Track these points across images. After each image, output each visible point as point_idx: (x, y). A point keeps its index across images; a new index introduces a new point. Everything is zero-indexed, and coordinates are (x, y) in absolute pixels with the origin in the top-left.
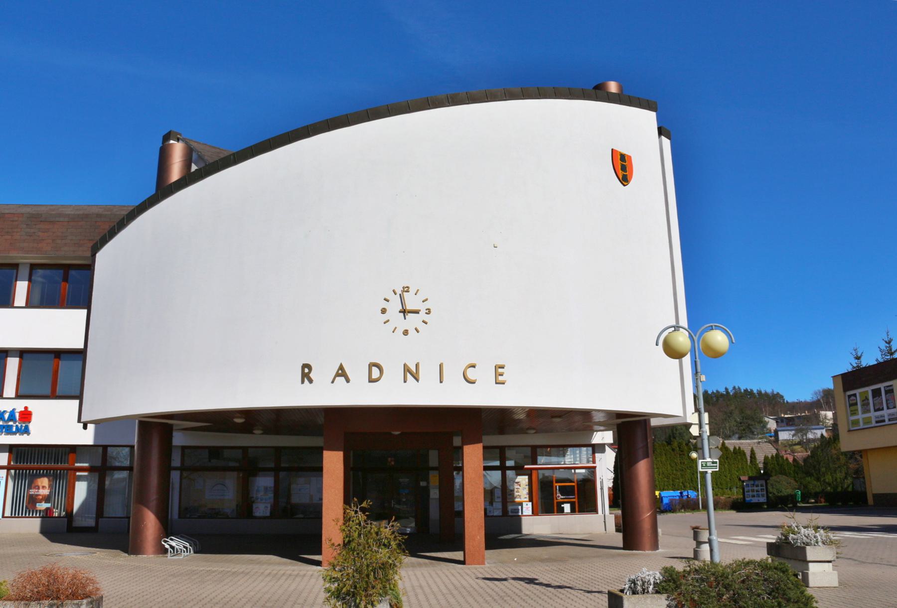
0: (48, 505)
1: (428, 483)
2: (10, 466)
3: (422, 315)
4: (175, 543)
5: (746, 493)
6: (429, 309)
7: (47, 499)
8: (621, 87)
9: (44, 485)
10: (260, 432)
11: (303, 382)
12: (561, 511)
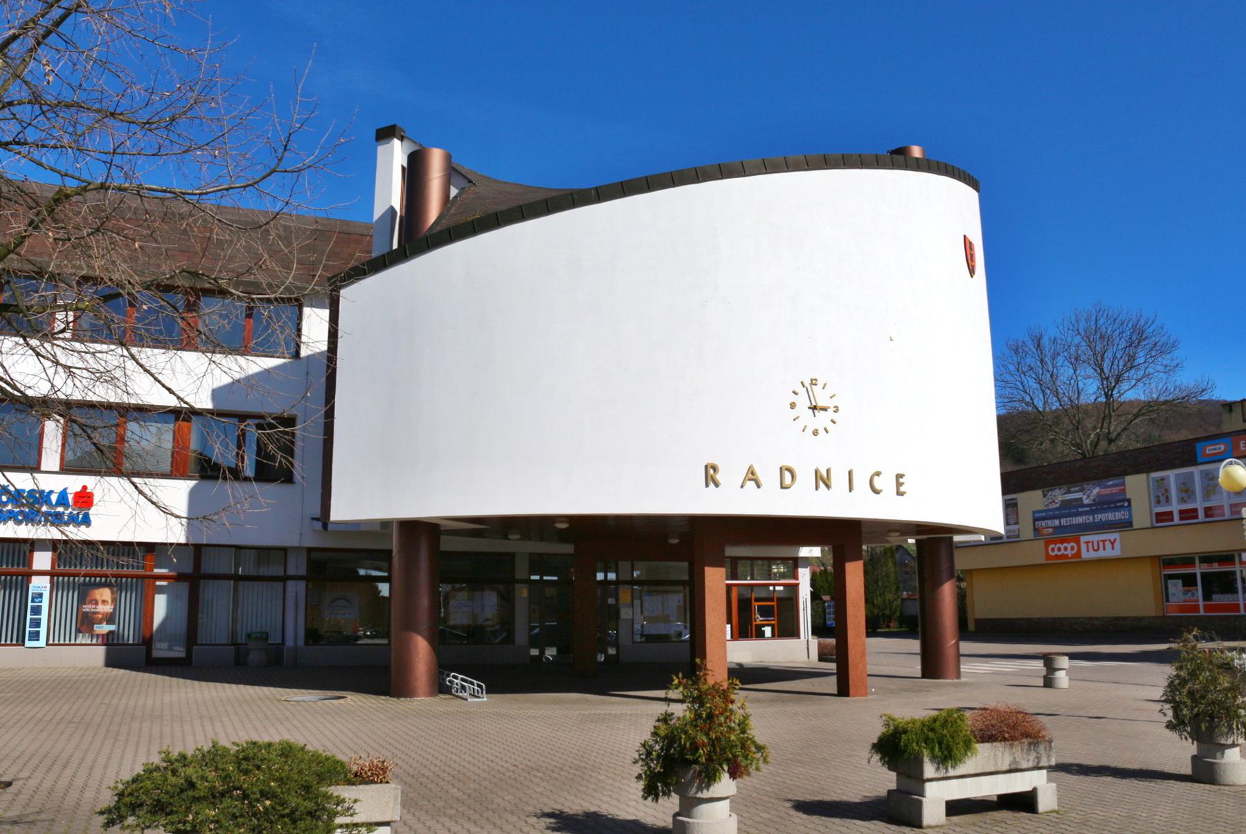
0: (112, 627)
1: (617, 600)
2: (54, 571)
3: (830, 414)
4: (456, 680)
5: (827, 616)
6: (837, 407)
7: (110, 619)
8: (924, 152)
9: (104, 598)
10: (518, 537)
11: (707, 485)
12: (760, 635)
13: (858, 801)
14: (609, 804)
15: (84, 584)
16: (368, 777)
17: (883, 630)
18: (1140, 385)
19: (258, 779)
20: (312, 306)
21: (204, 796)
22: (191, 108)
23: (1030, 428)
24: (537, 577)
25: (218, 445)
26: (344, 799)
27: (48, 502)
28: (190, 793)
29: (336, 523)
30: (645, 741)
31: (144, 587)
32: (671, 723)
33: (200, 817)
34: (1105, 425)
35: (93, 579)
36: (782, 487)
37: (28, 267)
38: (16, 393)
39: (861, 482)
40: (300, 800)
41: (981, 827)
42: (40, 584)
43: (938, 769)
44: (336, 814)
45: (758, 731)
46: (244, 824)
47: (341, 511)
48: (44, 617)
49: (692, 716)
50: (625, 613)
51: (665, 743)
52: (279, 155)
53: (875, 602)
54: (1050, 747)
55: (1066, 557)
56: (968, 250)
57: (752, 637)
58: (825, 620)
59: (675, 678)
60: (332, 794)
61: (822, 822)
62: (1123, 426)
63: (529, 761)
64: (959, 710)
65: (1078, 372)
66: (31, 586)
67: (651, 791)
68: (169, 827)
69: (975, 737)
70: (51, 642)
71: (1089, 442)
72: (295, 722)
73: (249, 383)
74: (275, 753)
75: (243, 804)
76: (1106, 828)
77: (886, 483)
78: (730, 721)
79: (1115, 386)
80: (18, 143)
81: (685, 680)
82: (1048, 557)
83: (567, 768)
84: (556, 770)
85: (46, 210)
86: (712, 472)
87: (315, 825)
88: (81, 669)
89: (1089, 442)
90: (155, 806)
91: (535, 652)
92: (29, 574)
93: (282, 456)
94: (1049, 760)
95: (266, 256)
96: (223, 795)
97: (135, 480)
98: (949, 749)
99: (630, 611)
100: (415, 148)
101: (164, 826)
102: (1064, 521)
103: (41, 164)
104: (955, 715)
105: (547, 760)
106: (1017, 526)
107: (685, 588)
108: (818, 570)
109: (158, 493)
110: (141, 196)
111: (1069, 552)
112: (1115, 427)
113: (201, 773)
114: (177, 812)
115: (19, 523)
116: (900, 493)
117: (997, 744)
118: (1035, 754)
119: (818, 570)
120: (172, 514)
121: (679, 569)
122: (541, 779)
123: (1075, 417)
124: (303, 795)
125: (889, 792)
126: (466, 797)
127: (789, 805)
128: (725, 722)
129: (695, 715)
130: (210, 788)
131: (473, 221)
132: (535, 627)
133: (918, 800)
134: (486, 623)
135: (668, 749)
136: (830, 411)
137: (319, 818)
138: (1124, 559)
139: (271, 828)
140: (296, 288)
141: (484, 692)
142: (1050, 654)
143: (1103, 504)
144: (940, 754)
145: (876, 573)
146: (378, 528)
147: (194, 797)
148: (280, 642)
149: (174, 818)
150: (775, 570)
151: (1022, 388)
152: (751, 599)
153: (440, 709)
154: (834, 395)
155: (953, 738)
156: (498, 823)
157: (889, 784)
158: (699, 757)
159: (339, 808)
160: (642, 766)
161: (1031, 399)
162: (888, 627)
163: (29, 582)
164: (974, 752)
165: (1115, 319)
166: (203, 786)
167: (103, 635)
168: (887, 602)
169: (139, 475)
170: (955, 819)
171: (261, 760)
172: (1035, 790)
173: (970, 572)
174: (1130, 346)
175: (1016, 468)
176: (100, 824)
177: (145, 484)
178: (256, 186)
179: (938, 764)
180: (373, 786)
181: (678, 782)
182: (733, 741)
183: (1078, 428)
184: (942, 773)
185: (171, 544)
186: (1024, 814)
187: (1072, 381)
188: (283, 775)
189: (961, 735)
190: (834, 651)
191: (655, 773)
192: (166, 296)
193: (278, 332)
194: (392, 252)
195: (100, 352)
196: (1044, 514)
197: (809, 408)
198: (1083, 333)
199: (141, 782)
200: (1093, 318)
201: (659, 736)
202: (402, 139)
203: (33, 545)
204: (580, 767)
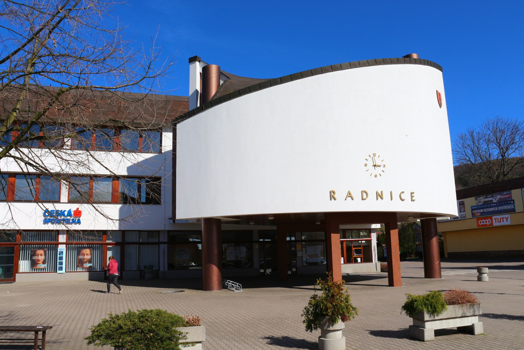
0: (91, 265)
1: (296, 248)
2: (67, 242)
3: (382, 168)
4: (230, 283)
6: (384, 165)
7: (90, 261)
8: (418, 56)
9: (87, 253)
10: (253, 223)
11: (331, 200)
13: (397, 330)
14: (292, 333)
15: (79, 247)
16: (192, 323)
17: (408, 258)
18: (517, 151)
19: (147, 325)
20: (166, 132)
21: (126, 332)
22: (112, 54)
23: (469, 171)
24: (262, 240)
25: (126, 190)
26: (182, 332)
27: (64, 215)
28: (120, 331)
29: (178, 220)
30: (306, 307)
31: (103, 248)
32: (317, 299)
33: (125, 340)
34: (502, 168)
35: (80, 245)
36: (362, 199)
37: (50, 121)
38: (46, 172)
39: (396, 196)
40: (164, 333)
41: (450, 341)
42: (62, 248)
43: (430, 317)
44: (179, 339)
45: (353, 302)
46: (142, 343)
47: (180, 215)
48: (64, 261)
49: (325, 296)
50: (299, 254)
51: (314, 308)
52: (147, 71)
53: (405, 246)
54: (479, 307)
55: (486, 225)
56: (439, 97)
57: (352, 262)
58: (383, 254)
59: (318, 280)
60: (177, 331)
61: (381, 339)
62: (510, 169)
63: (260, 316)
64: (439, 291)
65: (489, 146)
66: (58, 248)
67: (309, 327)
68: (112, 344)
69: (446, 303)
70: (67, 271)
71: (495, 176)
72: (164, 302)
73: (139, 164)
74: (154, 314)
75: (142, 335)
76: (505, 341)
77: (406, 196)
78: (341, 298)
79: (506, 152)
80: (43, 72)
81: (322, 281)
82: (478, 225)
83: (275, 318)
84: (270, 319)
85: (55, 98)
86: (333, 194)
87: (171, 343)
88: (79, 281)
89: (495, 176)
90: (107, 336)
91: (262, 271)
92: (58, 244)
93: (152, 193)
94: (479, 312)
95: (143, 112)
96: (133, 331)
97: (94, 205)
98: (435, 308)
99: (301, 253)
100: (205, 65)
101: (110, 344)
102: (485, 210)
103: (54, 80)
104: (437, 293)
105: (267, 315)
106: (464, 213)
107: (324, 243)
108: (380, 234)
109: (104, 210)
110: (92, 90)
111: (488, 223)
112: (506, 169)
113: (124, 323)
114: (115, 338)
115: (53, 223)
116: (412, 200)
117: (456, 306)
118: (473, 310)
119: (380, 234)
120: (109, 219)
121: (321, 235)
122: (264, 323)
123: (488, 166)
124: (165, 331)
125: (410, 326)
126: (233, 331)
127: (368, 332)
128: (339, 298)
129: (326, 296)
130: (128, 329)
131: (230, 94)
132: (262, 261)
133: (422, 329)
134: (242, 259)
135: (316, 310)
136: (382, 167)
137: (172, 340)
138: (512, 225)
139: (153, 344)
140: (156, 124)
141: (241, 287)
142: (480, 267)
143: (501, 203)
144: (431, 310)
145: (405, 234)
146: (195, 222)
147: (122, 332)
148: (158, 269)
149: (114, 341)
150: (362, 234)
151: (465, 154)
152: (351, 247)
153: (223, 295)
154: (383, 160)
155: (436, 303)
156: (247, 342)
157: (410, 323)
158: (328, 313)
159: (180, 336)
160: (305, 317)
161: (469, 159)
162: (411, 257)
163: (58, 247)
164: (446, 309)
165: (506, 123)
166: (125, 328)
167: (87, 268)
168: (410, 246)
169: (96, 203)
170: (439, 337)
171: (148, 317)
172: (473, 325)
173: (445, 233)
174: (512, 134)
175: (464, 188)
176: (86, 343)
177: (99, 206)
178: (138, 84)
179: (430, 314)
180: (194, 327)
181: (320, 323)
182: (343, 306)
183: (490, 170)
184: (432, 318)
185: (109, 230)
186: (469, 335)
187: (487, 150)
188: (157, 323)
189: (440, 302)
190: (387, 268)
191: (310, 320)
192: (104, 130)
193: (149, 143)
194: (197, 108)
195: (80, 154)
196: (476, 207)
197: (373, 166)
198: (491, 129)
199: (101, 326)
200: (496, 123)
201: (311, 304)
202: (199, 61)
203: (58, 232)
204: (281, 318)
